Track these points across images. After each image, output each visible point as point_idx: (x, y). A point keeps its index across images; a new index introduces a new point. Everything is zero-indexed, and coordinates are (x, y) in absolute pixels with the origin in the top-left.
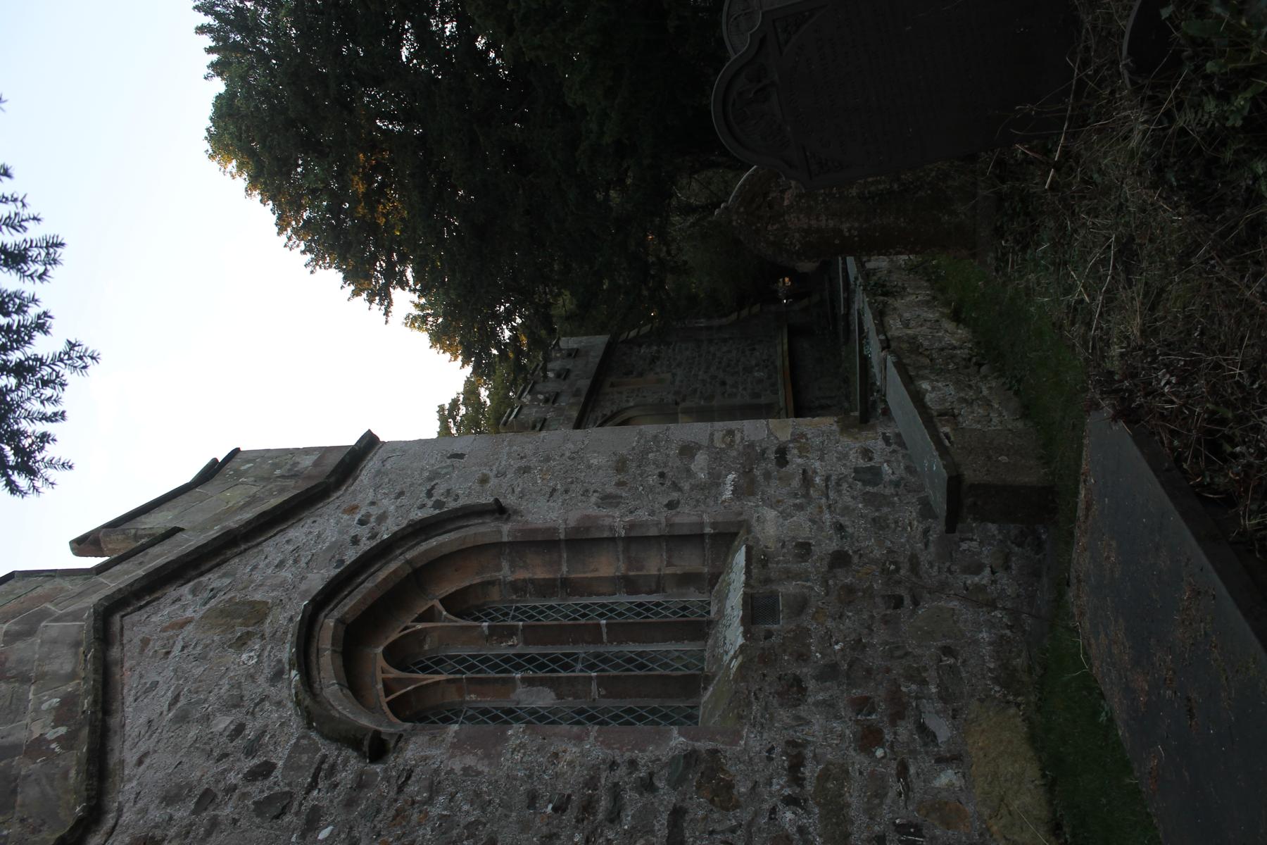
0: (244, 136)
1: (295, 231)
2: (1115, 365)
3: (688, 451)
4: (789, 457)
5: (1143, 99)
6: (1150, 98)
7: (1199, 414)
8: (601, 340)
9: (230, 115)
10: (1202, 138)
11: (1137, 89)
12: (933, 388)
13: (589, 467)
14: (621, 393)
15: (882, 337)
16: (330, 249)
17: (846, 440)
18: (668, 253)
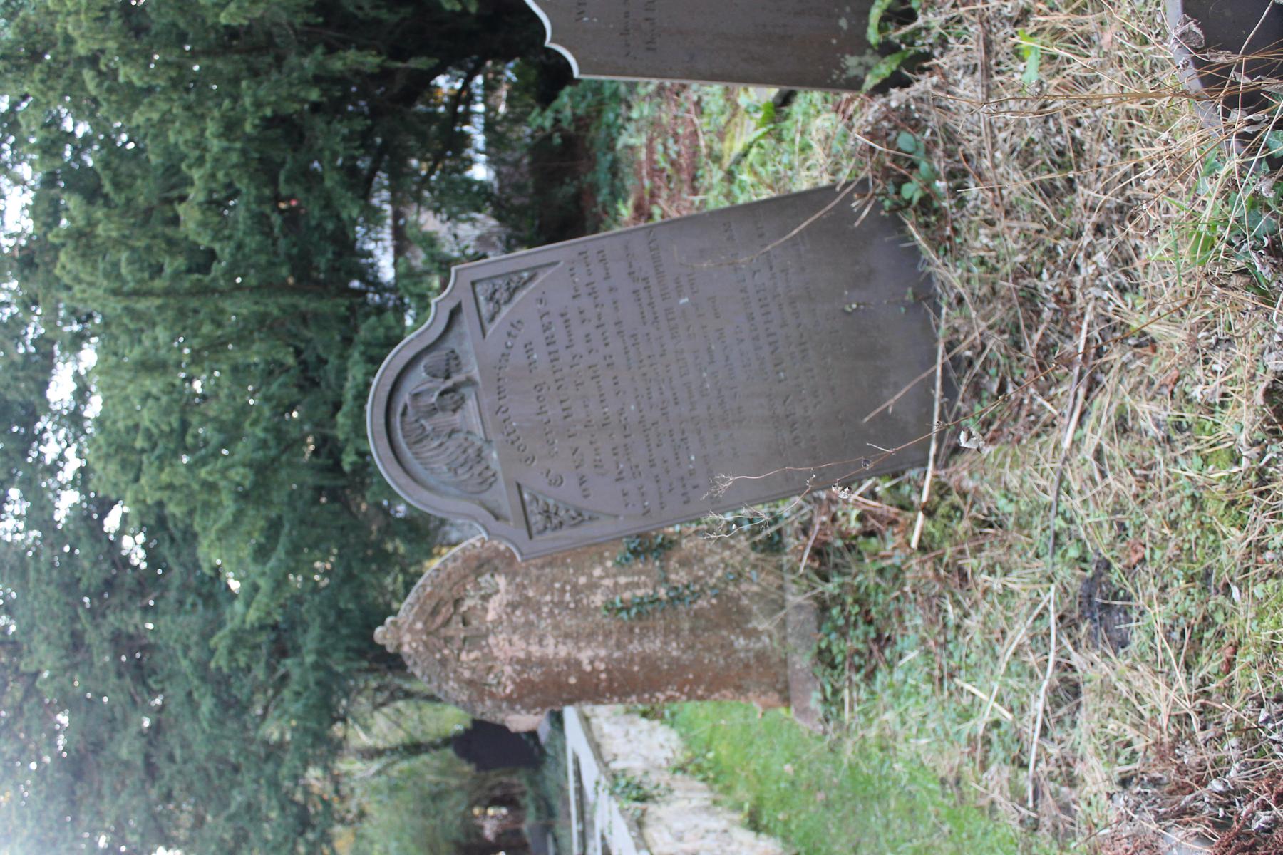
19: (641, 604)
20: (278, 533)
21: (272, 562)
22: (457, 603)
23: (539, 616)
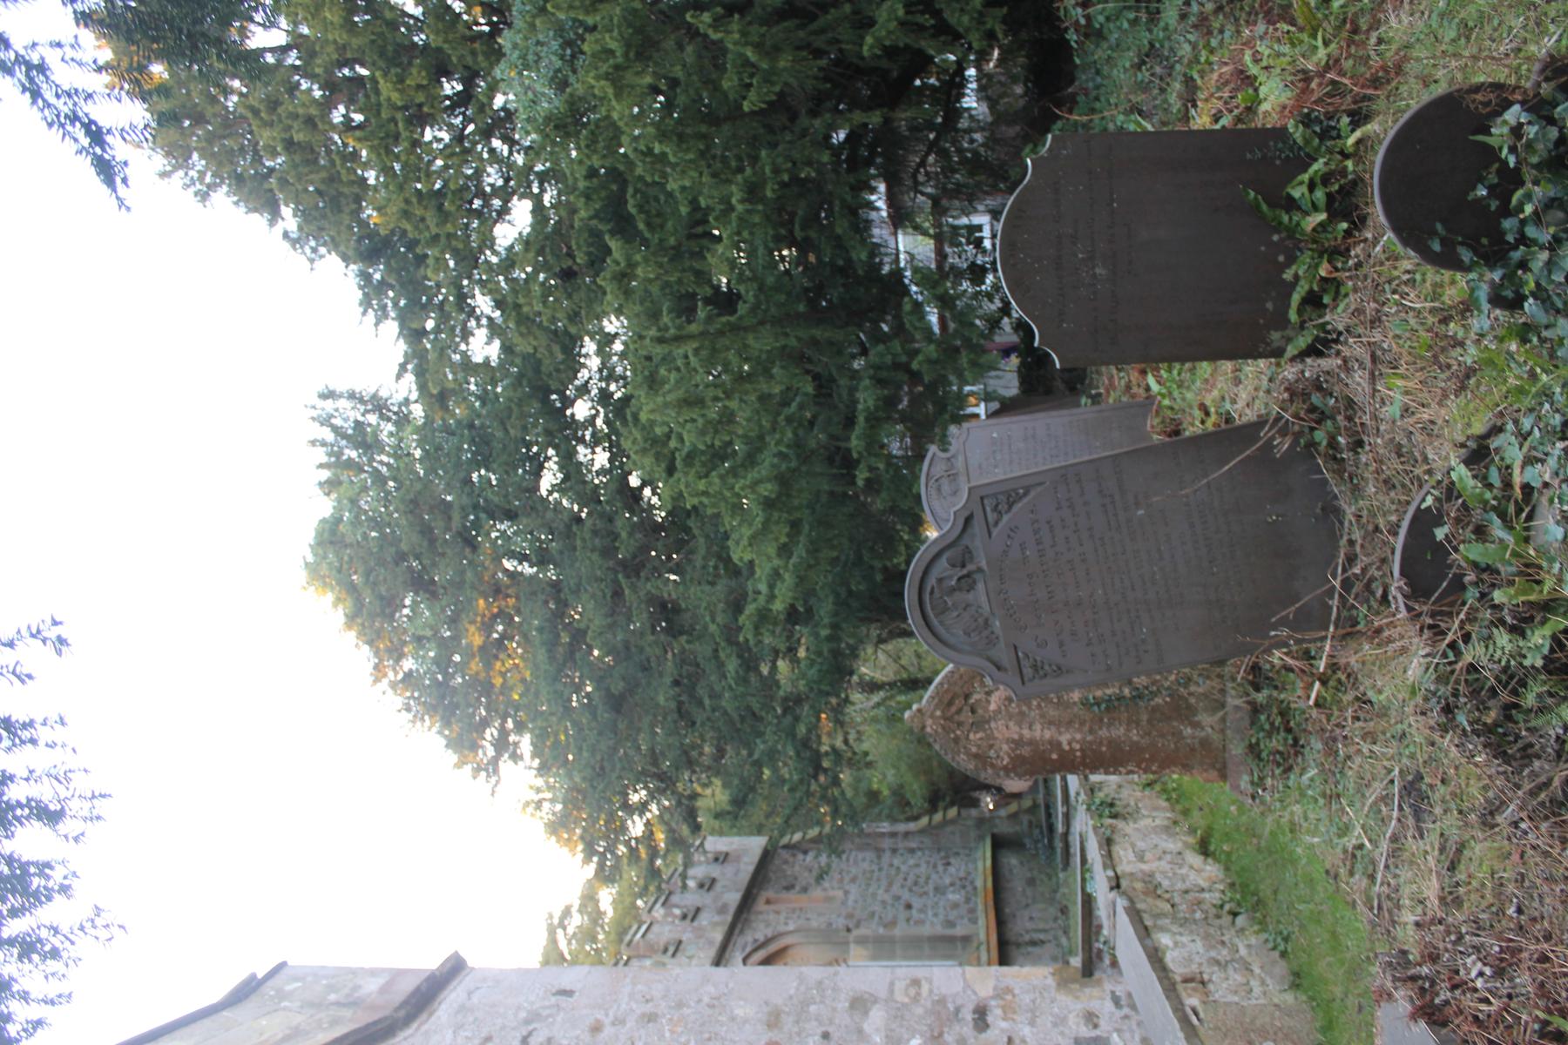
0: (345, 566)
1: (393, 685)
2: (1408, 937)
3: (860, 1004)
4: (990, 1019)
5: (1421, 630)
6: (1430, 627)
7: (1527, 1023)
8: (757, 844)
9: (331, 543)
10: (1496, 678)
11: (1415, 616)
12: (1176, 944)
13: (733, 1019)
14: (778, 913)
15: (1110, 873)
16: (431, 709)
17: (1064, 999)
18: (846, 742)
19: (1110, 700)
20: (799, 533)
21: (794, 560)
22: (967, 697)
23: (1030, 708)
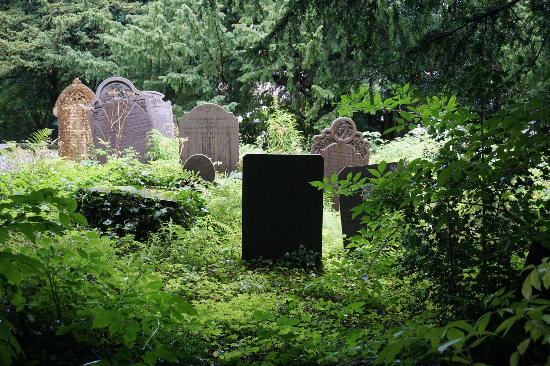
22: (84, 97)
